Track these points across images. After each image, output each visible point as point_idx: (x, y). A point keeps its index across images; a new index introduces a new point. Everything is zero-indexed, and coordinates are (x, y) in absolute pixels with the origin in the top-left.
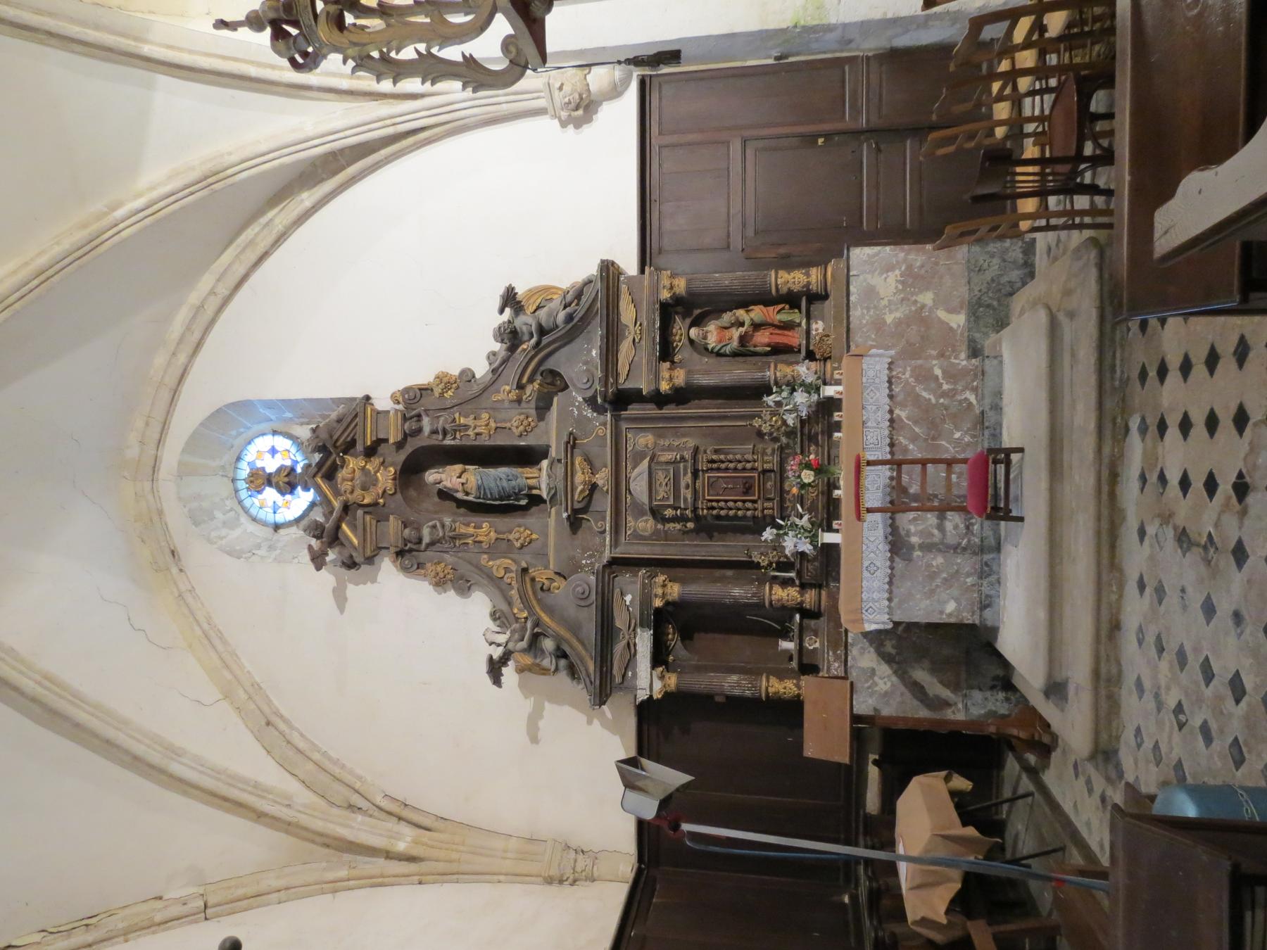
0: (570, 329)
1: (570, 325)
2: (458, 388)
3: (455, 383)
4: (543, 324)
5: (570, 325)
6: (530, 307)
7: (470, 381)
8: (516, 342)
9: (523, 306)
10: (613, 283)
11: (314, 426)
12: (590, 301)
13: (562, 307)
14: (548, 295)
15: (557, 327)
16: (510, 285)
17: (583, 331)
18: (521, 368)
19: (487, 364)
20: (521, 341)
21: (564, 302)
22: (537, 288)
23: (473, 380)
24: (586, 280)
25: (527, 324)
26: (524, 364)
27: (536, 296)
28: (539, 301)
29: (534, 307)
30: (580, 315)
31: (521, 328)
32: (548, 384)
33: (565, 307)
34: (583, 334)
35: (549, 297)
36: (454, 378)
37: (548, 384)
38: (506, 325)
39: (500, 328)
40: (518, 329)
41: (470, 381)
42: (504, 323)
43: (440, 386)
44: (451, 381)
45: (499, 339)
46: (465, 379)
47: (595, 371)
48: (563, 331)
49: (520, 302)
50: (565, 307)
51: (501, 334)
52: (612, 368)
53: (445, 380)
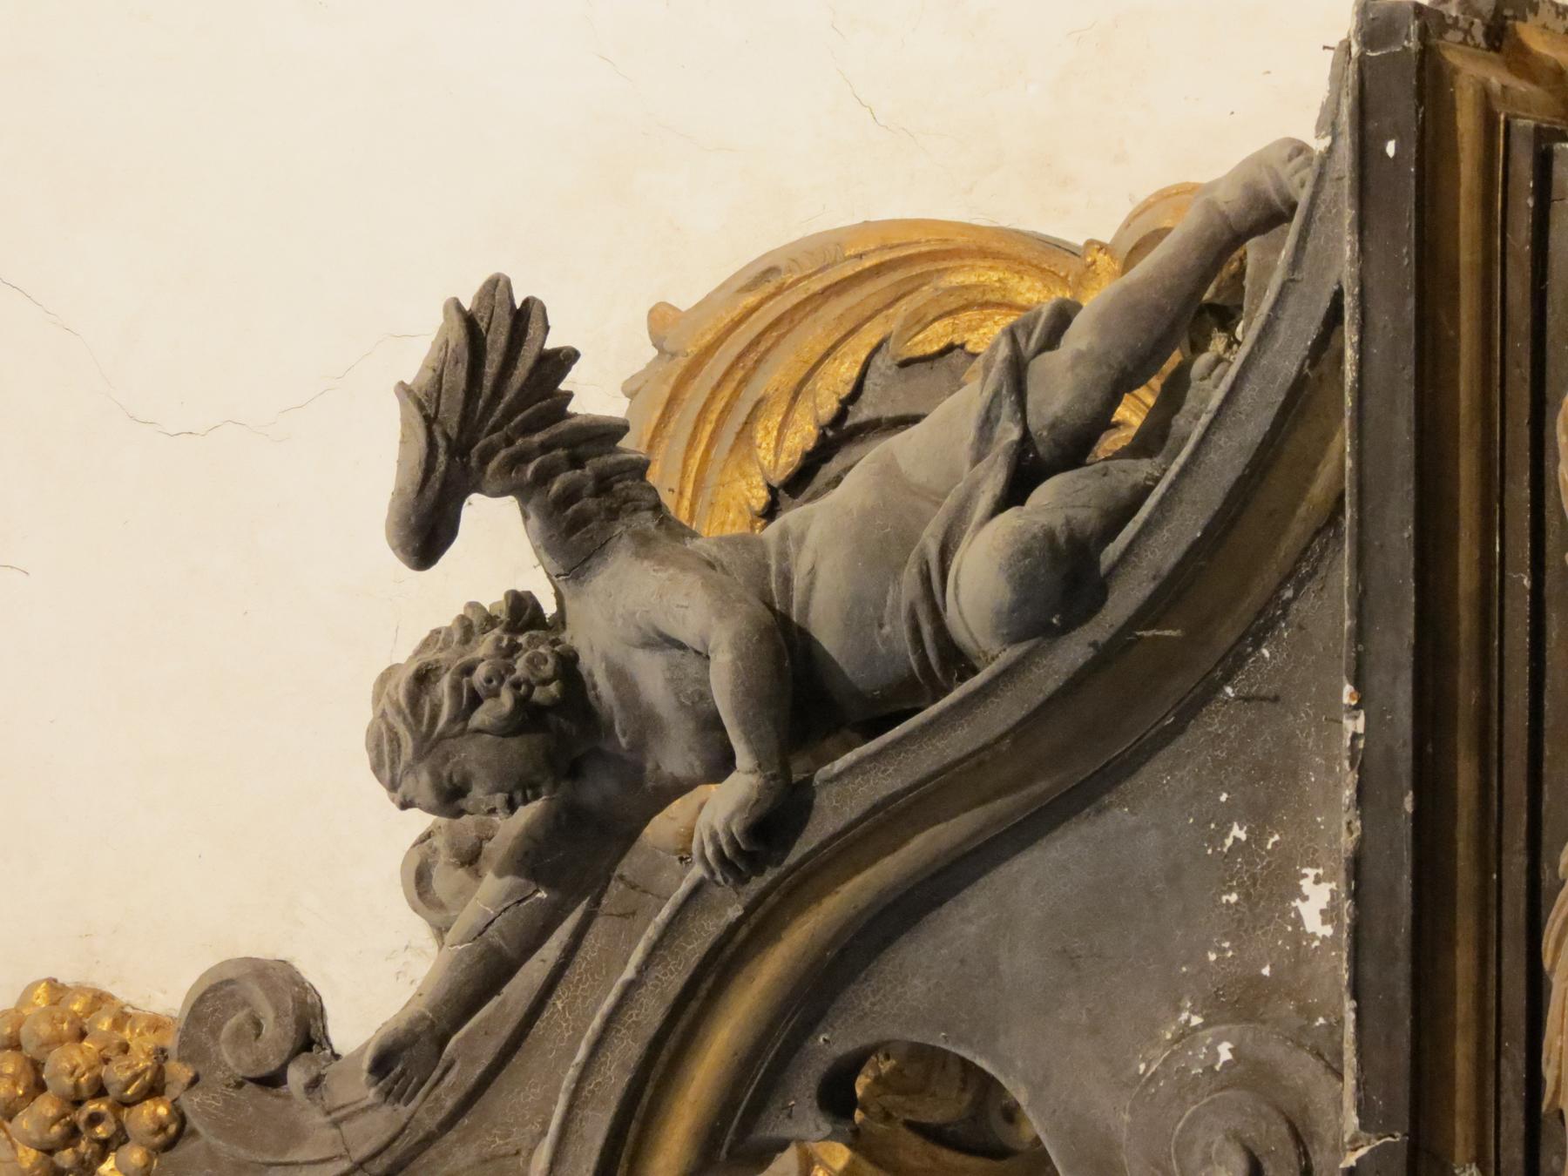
0: (1077, 683)
1: (1074, 651)
2: (175, 1135)
3: (154, 1090)
4: (827, 632)
5: (1074, 651)
6: (764, 437)
7: (273, 1081)
8: (598, 789)
9: (639, 469)
10: (1493, 223)
11: (549, 608)
12: (1253, 425)
13: (993, 481)
14: (919, 322)
15: (957, 661)
16: (496, 287)
17: (1208, 692)
18: (628, 1050)
19: (418, 929)
20: (632, 770)
21: (1009, 433)
22: (826, 248)
23: (297, 1076)
24: (1230, 199)
25: (665, 642)
26: (650, 1012)
27: (811, 337)
28: (844, 371)
29: (803, 435)
30: (1165, 552)
31: (620, 677)
32: (932, 1134)
33: (1015, 492)
34: (1213, 722)
35: (931, 340)
36: (142, 1047)
37: (932, 1134)
38: (485, 646)
39: (423, 678)
40: (603, 687)
41: (273, 1081)
42: (471, 626)
43: (25, 1122)
44: (117, 1074)
45: (421, 783)
46: (232, 1059)
47: (1321, 1096)
48: (1003, 714)
49: (607, 434)
50: (1015, 492)
51: (429, 745)
52: (1488, 1065)
53: (66, 1066)
